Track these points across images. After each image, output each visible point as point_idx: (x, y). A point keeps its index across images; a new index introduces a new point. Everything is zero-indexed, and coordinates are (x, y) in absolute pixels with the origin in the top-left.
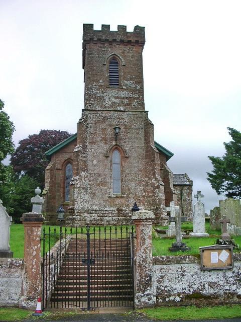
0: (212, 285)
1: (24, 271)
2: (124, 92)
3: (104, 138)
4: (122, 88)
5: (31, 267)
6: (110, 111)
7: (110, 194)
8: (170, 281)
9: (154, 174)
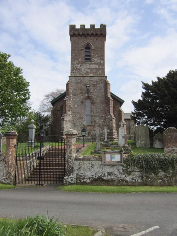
0: (109, 174)
1: (4, 163)
2: (93, 65)
3: (81, 92)
4: (92, 63)
5: (8, 161)
6: (85, 76)
7: (84, 124)
8: (85, 169)
9: (110, 112)
